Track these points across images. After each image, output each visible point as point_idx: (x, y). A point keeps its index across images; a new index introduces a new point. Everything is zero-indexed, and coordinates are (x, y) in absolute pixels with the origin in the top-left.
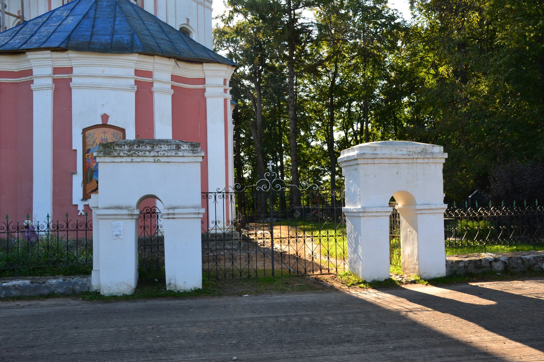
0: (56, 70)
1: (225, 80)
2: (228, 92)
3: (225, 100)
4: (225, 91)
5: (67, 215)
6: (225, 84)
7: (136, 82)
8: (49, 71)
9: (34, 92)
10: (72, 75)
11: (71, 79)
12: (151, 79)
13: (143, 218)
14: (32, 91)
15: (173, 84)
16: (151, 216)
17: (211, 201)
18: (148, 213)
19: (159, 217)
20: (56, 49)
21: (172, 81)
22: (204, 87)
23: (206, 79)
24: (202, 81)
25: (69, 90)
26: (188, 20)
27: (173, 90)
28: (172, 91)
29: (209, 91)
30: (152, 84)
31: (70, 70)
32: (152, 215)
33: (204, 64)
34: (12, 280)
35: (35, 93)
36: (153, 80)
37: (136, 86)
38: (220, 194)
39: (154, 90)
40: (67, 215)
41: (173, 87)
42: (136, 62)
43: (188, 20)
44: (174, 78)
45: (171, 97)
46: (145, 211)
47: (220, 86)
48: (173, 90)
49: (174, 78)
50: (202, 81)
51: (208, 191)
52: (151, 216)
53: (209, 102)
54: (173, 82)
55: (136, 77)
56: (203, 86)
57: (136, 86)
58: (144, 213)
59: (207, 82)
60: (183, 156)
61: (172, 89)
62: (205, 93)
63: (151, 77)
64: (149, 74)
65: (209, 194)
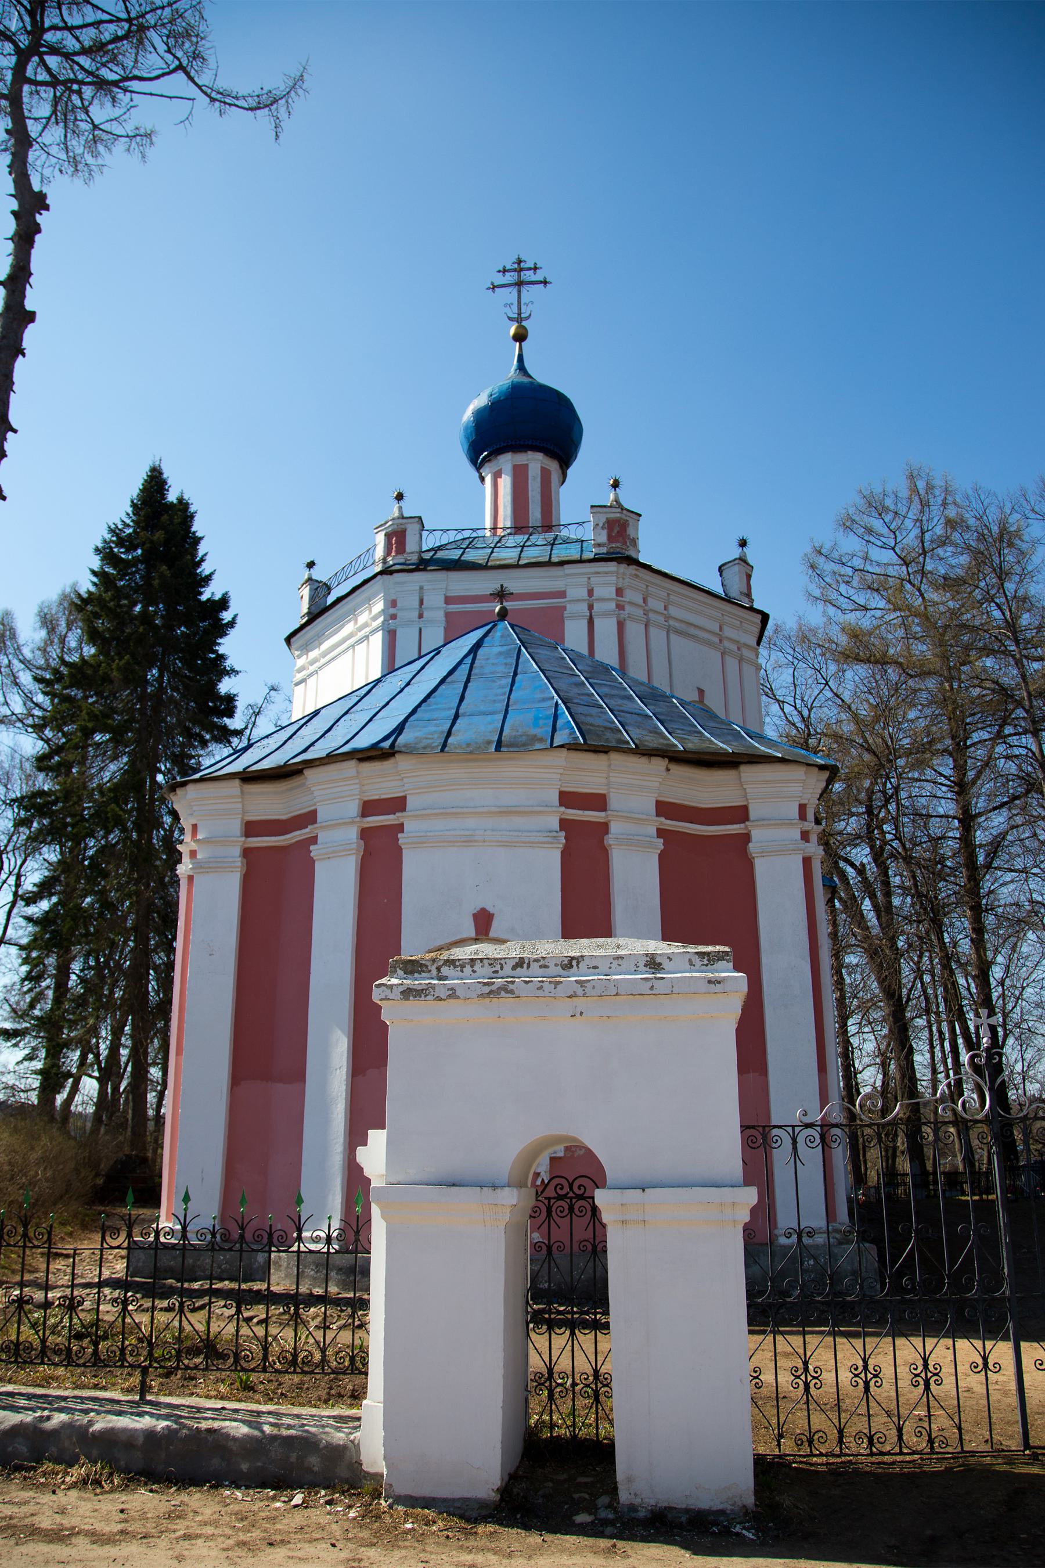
0: (368, 808)
1: (802, 808)
2: (814, 838)
3: (807, 862)
4: (805, 836)
5: (187, 1199)
6: (803, 816)
7: (564, 824)
8: (353, 808)
9: (317, 864)
10: (404, 814)
11: (402, 825)
12: (603, 814)
13: (544, 1214)
14: (314, 862)
15: (661, 824)
16: (571, 1209)
17: (781, 1155)
18: (560, 1198)
19: (554, 1214)
20: (370, 754)
21: (658, 815)
22: (746, 827)
23: (751, 808)
24: (741, 814)
25: (397, 854)
26: (701, 692)
27: (662, 840)
28: (660, 843)
29: (760, 837)
30: (604, 828)
31: (399, 804)
32: (576, 1207)
33: (743, 768)
34: (125, 1430)
35: (319, 867)
36: (607, 816)
37: (563, 834)
38: (809, 1131)
39: (611, 842)
40: (187, 1199)
41: (661, 833)
42: (561, 771)
43: (701, 692)
44: (663, 809)
45: (656, 858)
46: (550, 1192)
47: (789, 823)
48: (662, 840)
49: (663, 809)
50: (741, 814)
51: (769, 1117)
52: (571, 1209)
53: (761, 867)
54: (662, 819)
55: (563, 809)
56: (742, 825)
57: (563, 834)
58: (549, 1199)
59: (753, 815)
60: (549, 564)
61: (658, 836)
62: (750, 845)
63: (603, 808)
64: (599, 802)
65: (775, 1132)
